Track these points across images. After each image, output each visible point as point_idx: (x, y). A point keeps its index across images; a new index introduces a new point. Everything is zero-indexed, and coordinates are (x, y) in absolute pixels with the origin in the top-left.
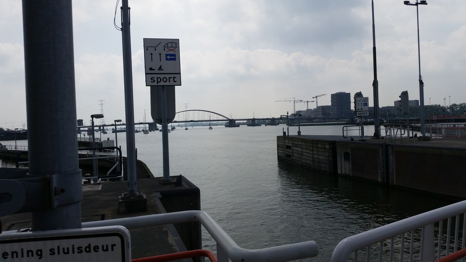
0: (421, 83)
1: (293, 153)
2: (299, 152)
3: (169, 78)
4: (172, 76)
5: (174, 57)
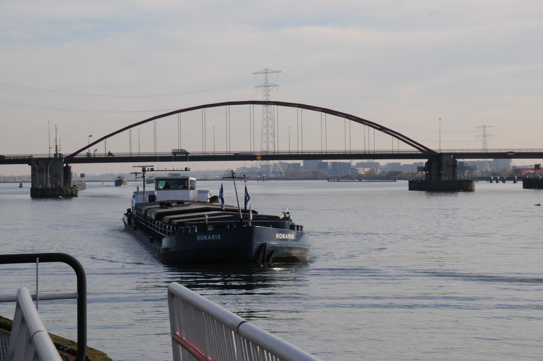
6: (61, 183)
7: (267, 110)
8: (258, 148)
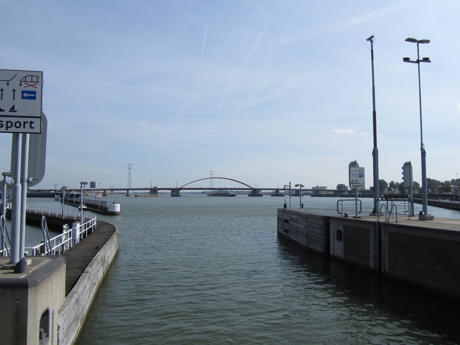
0: (423, 153)
1: (290, 227)
2: (295, 227)
3: (25, 123)
4: (29, 120)
5: (34, 95)
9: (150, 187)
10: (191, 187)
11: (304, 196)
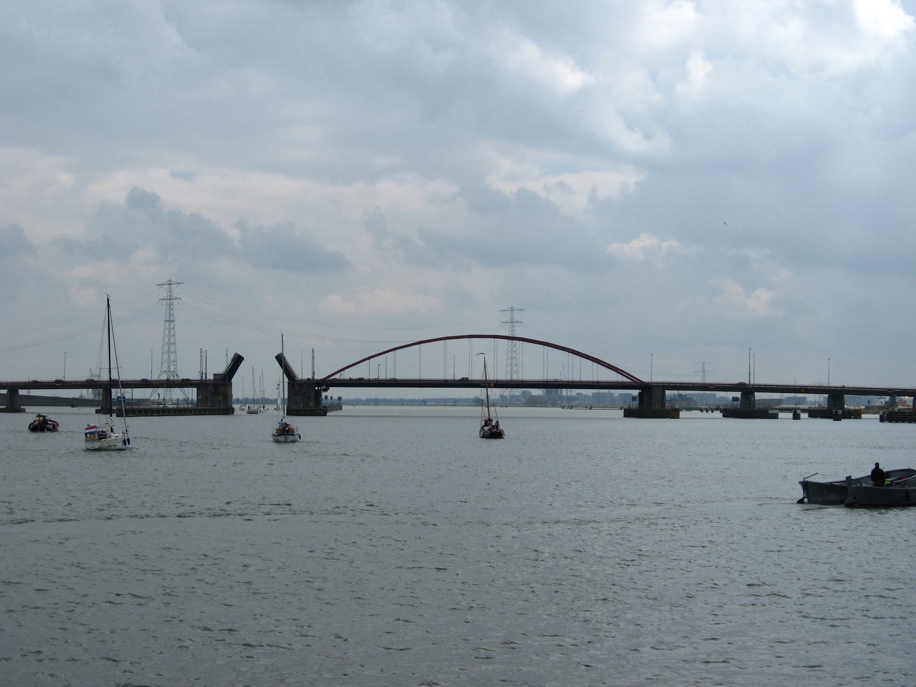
6: (312, 404)
7: (512, 343)
8: (477, 375)
9: (195, 376)
10: (382, 377)
11: (863, 416)
